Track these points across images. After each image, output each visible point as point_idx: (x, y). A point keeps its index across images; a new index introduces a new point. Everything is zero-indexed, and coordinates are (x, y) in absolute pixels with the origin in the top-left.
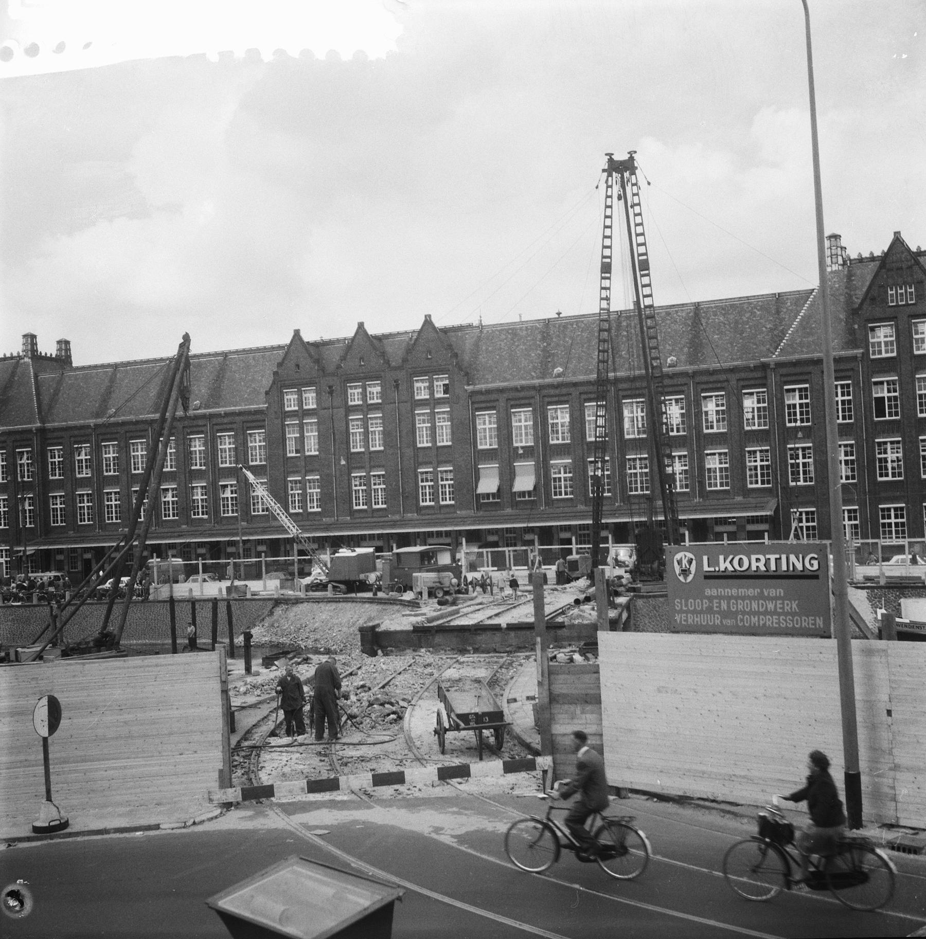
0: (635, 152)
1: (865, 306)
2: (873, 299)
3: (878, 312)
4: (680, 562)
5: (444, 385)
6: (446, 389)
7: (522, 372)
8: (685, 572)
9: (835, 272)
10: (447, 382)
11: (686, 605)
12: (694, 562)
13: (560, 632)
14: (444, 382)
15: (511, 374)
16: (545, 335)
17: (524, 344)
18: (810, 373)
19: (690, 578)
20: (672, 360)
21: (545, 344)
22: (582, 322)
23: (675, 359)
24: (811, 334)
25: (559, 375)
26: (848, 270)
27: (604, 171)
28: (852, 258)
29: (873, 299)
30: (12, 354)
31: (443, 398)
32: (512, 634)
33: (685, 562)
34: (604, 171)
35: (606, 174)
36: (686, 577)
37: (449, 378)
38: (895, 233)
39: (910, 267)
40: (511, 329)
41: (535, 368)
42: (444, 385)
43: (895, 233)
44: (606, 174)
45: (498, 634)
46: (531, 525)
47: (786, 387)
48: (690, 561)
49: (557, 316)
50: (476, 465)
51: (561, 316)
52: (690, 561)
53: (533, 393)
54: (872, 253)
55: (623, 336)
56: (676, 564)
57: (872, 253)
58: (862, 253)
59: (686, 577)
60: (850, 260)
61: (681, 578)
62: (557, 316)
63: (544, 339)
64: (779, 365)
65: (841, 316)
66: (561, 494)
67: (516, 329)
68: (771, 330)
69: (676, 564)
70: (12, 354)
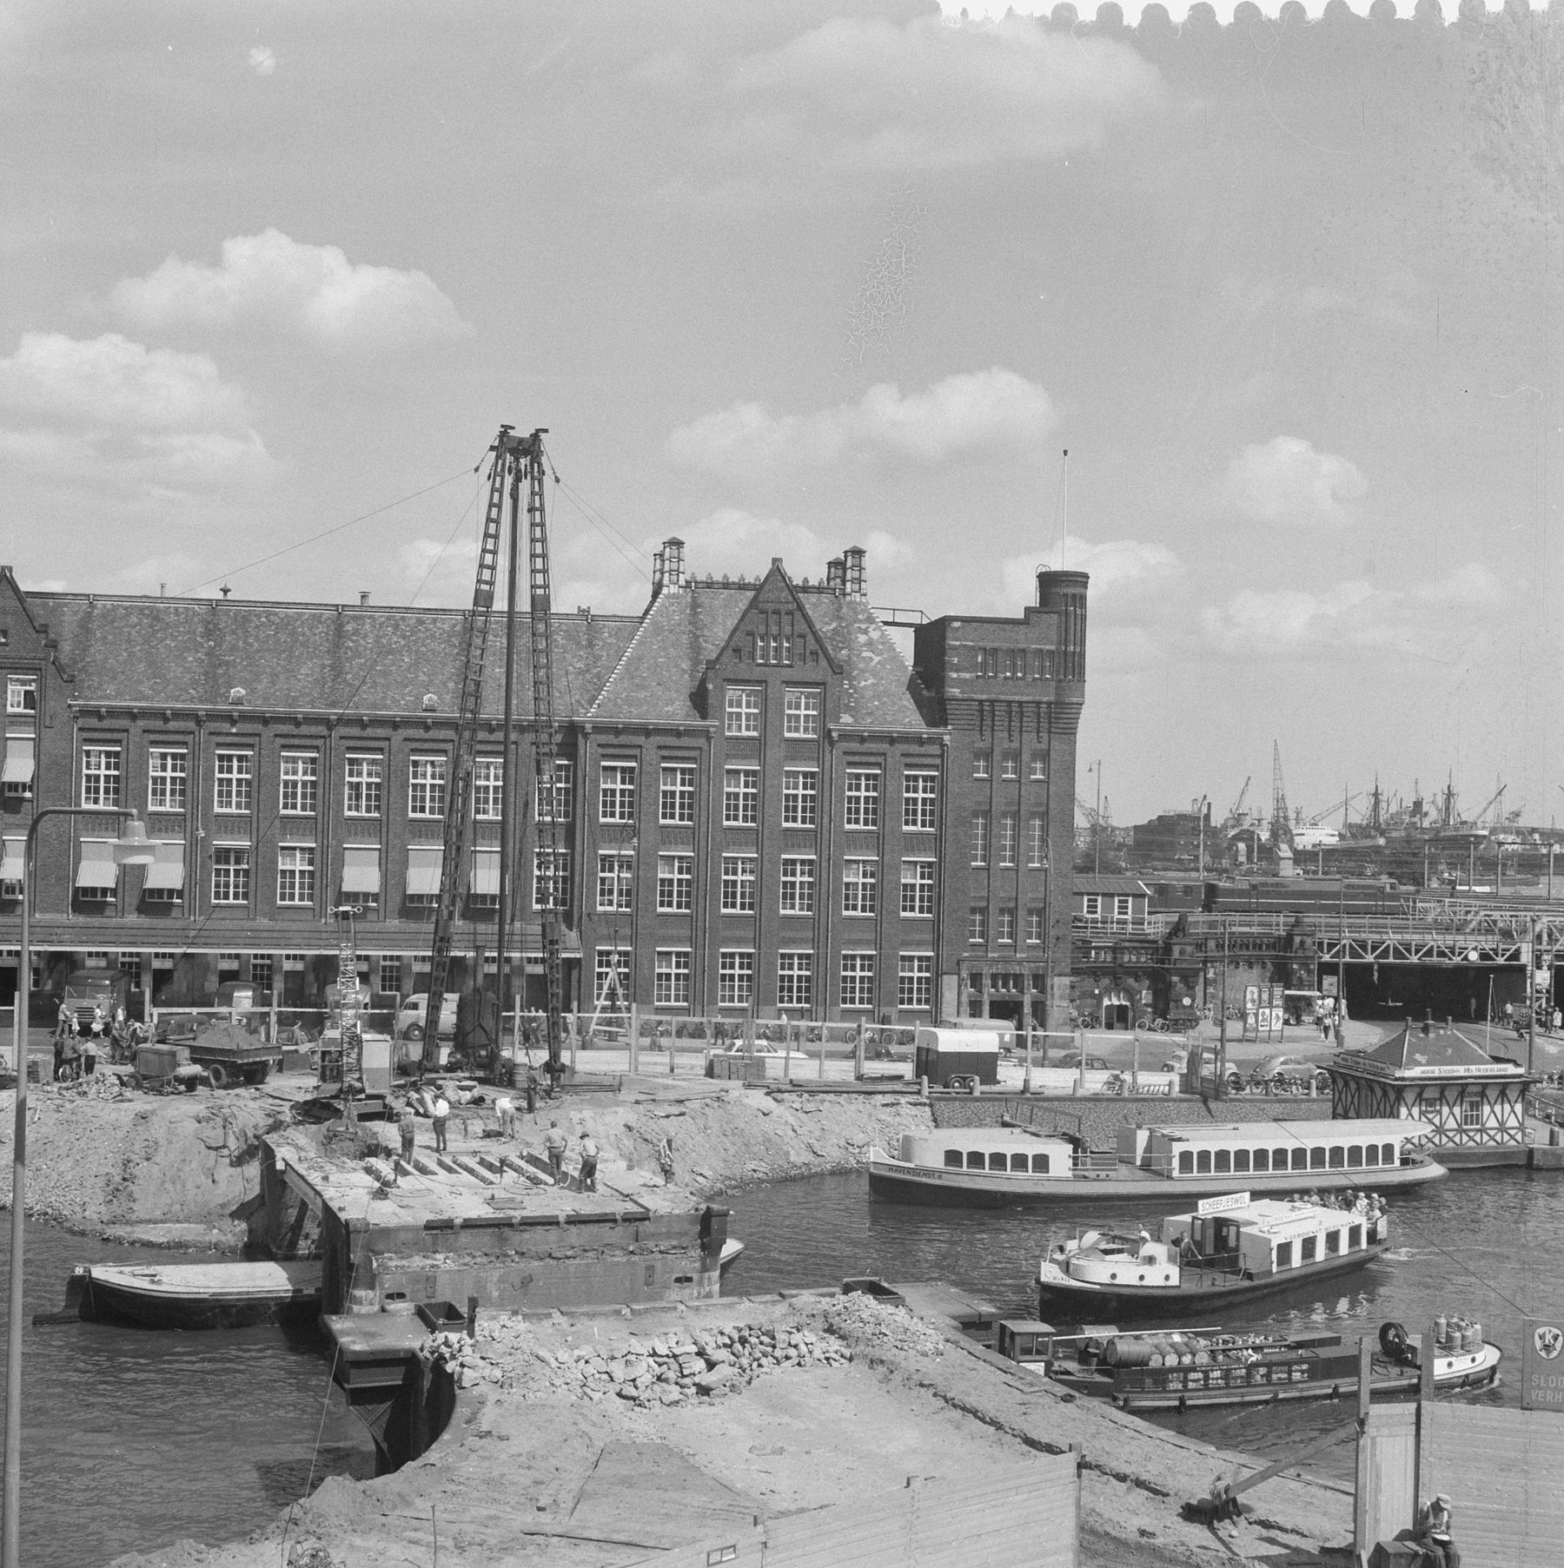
0: (546, 431)
1: (724, 659)
2: (737, 651)
3: (743, 670)
4: (1541, 1337)
5: (26, 692)
6: (30, 701)
7: (171, 687)
8: (1547, 1348)
9: (674, 596)
10: (32, 688)
11: (1546, 1381)
12: (1561, 1339)
13: (646, 1227)
14: (28, 688)
15: (151, 688)
16: (211, 626)
17: (174, 638)
18: (640, 747)
19: (1554, 1354)
20: (430, 699)
21: (212, 643)
22: (276, 614)
23: (435, 697)
24: (641, 687)
25: (239, 702)
26: (693, 597)
27: (492, 448)
28: (698, 579)
29: (737, 651)
30: (806, 580)
31: (21, 715)
32: (574, 1229)
33: (1549, 1338)
34: (492, 448)
35: (494, 454)
36: (1548, 1353)
37: (39, 682)
38: (775, 561)
39: (790, 613)
40: (148, 607)
41: (195, 683)
42: (26, 692)
43: (775, 561)
44: (494, 454)
45: (554, 1231)
46: (190, 951)
47: (603, 763)
48: (1556, 1338)
49: (220, 596)
50: (77, 837)
51: (230, 596)
52: (1556, 1338)
53: (884, 747)
54: (725, 576)
55: (347, 648)
56: (1537, 1337)
57: (725, 576)
58: (696, 572)
59: (1548, 1353)
60: (696, 582)
61: (1543, 1354)
62: (220, 596)
63: (208, 634)
64: (599, 729)
65: (684, 666)
66: (292, 898)
67: (158, 610)
68: (581, 672)
69: (1537, 1337)
70: (806, 580)
